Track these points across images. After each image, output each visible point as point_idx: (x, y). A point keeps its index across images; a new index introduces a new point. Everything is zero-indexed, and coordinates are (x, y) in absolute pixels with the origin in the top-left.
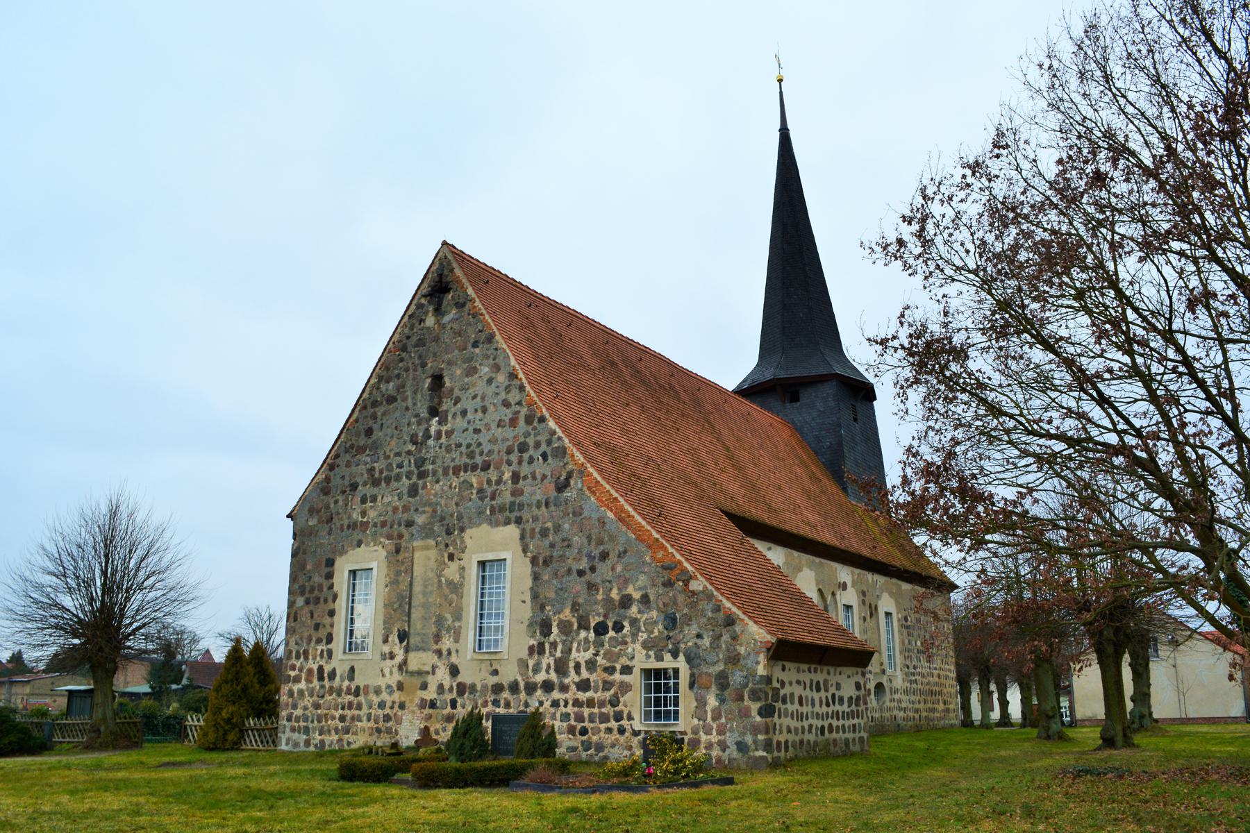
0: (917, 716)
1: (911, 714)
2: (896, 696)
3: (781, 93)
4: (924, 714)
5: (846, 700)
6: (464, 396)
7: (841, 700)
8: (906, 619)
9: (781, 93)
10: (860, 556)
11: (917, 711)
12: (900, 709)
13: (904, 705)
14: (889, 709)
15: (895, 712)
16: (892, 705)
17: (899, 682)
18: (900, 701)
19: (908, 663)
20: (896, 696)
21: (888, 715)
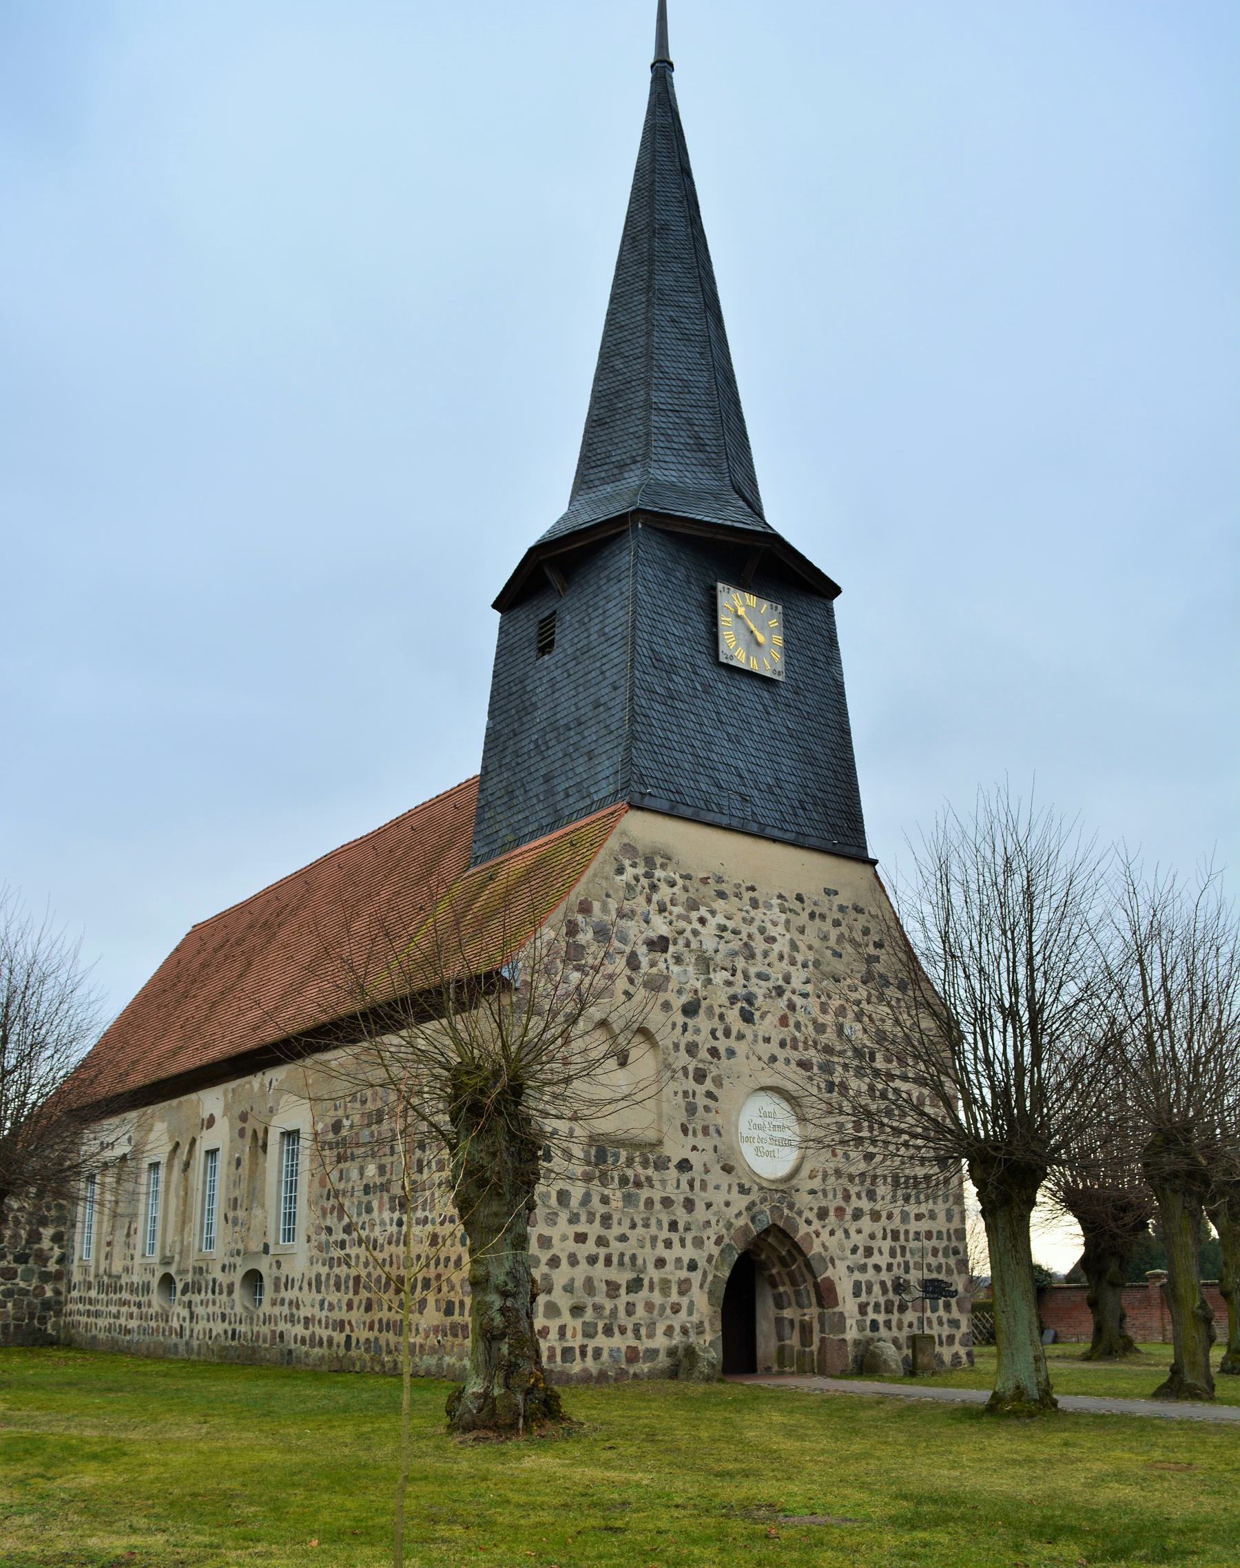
0: (339, 1338)
1: (325, 1333)
2: (289, 1295)
3: (662, 69)
4: (363, 1334)
5: (287, 1302)
6: (762, 910)
7: (282, 1302)
8: (337, 1127)
9: (662, 69)
10: (276, 1062)
11: (340, 1326)
12: (292, 1319)
13: (304, 1312)
14: (267, 1319)
15: (282, 1326)
16: (276, 1310)
17: (300, 1260)
18: (295, 1304)
19: (331, 1221)
20: (289, 1295)
21: (265, 1330)
